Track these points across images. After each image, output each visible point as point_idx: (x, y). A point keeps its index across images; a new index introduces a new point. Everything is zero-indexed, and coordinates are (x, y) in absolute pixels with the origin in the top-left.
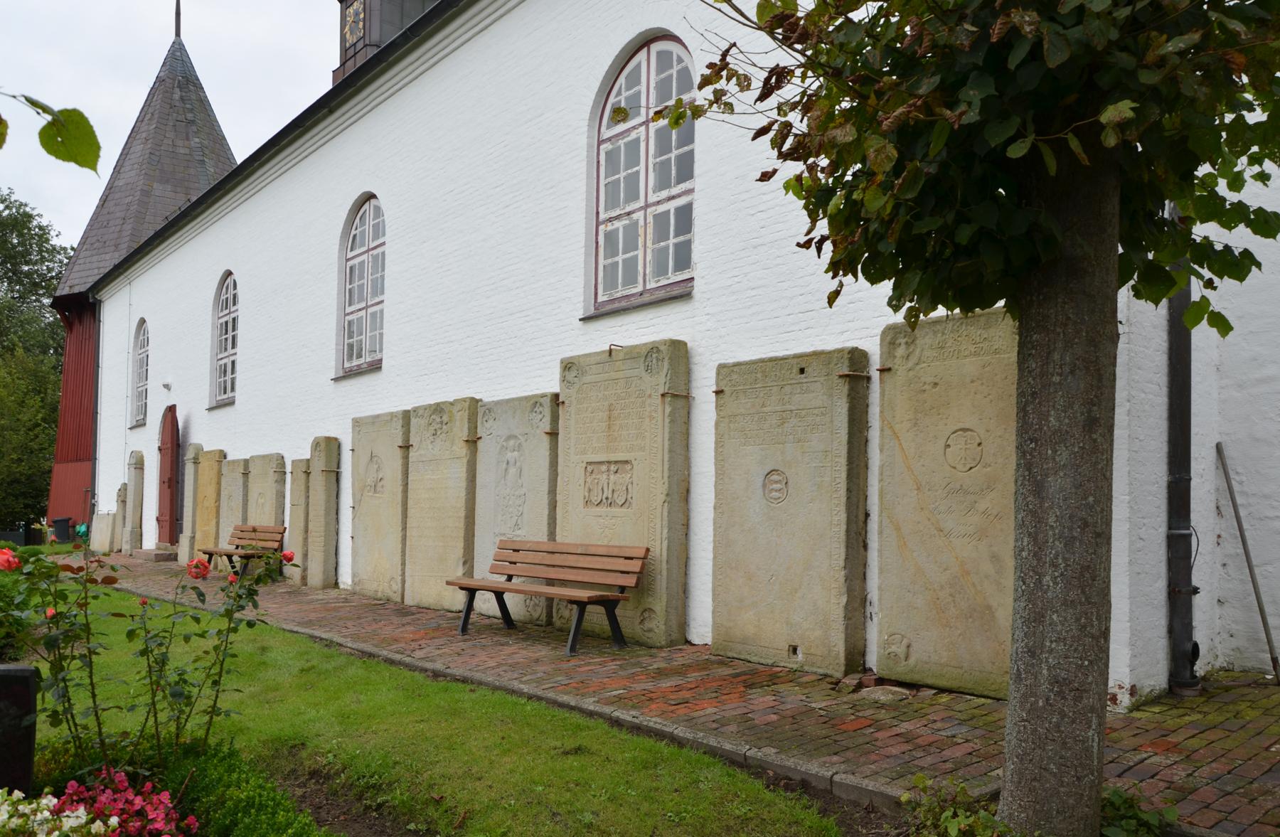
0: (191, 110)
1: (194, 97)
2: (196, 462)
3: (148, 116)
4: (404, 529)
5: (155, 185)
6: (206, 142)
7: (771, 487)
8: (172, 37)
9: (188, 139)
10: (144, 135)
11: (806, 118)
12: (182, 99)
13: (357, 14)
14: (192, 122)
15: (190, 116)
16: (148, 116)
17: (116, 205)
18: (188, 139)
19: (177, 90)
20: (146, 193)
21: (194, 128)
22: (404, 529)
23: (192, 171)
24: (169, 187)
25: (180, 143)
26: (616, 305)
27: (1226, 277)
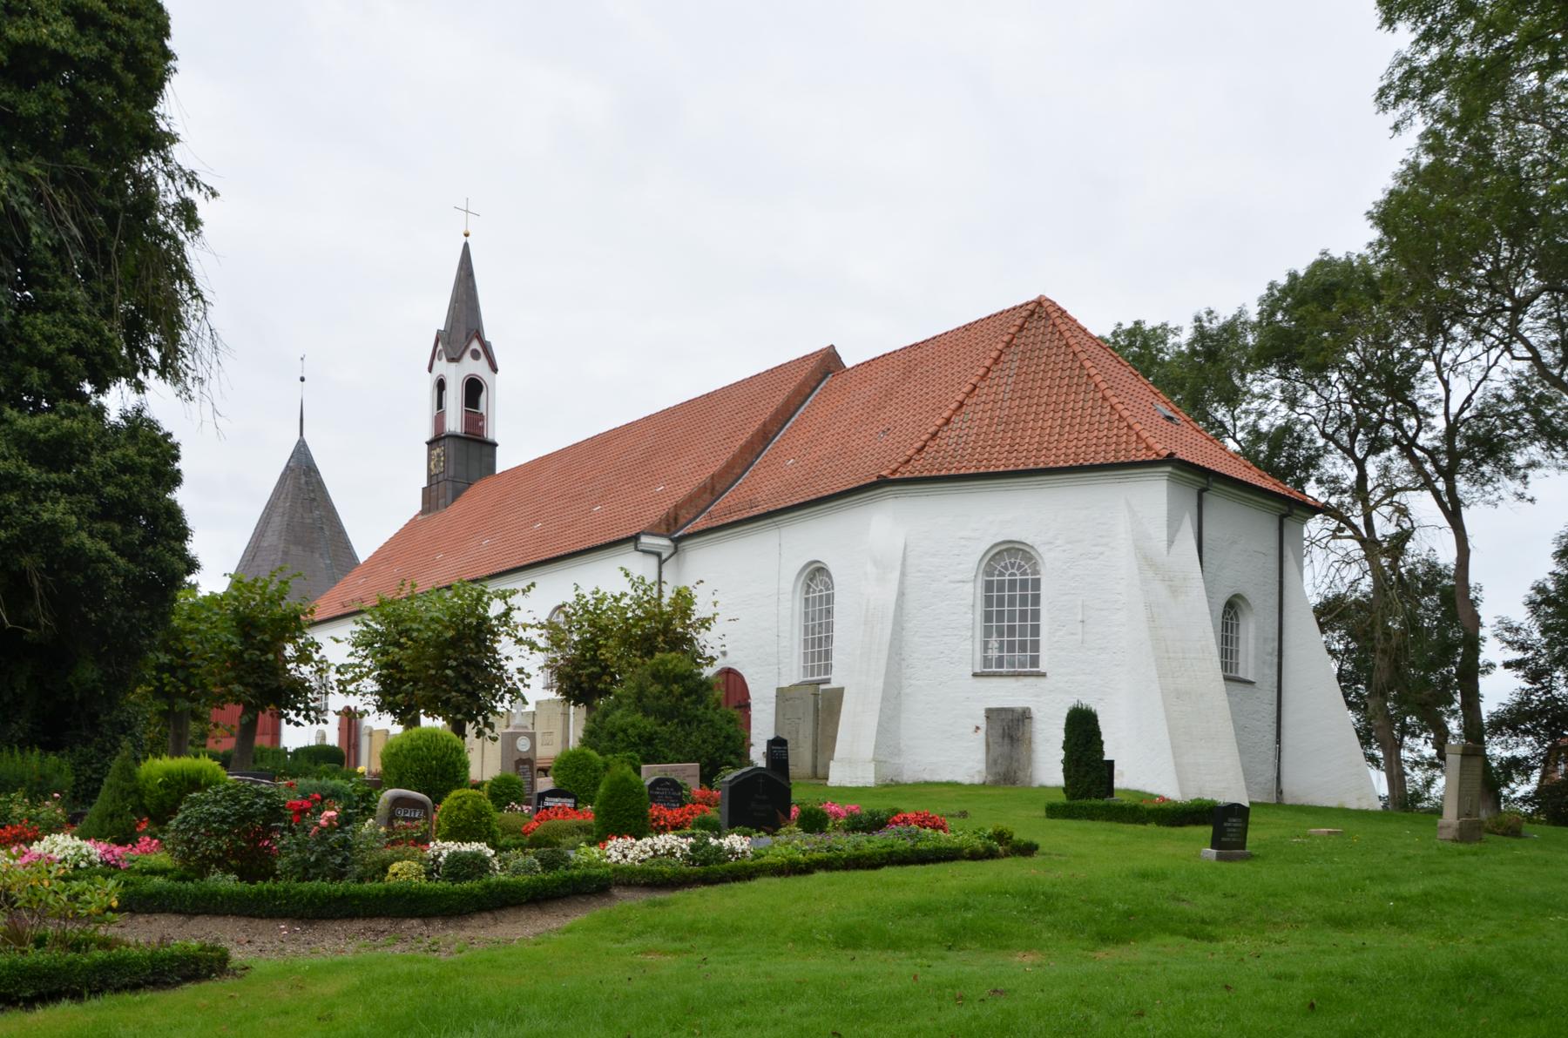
0: (313, 491)
1: (314, 480)
2: (370, 735)
3: (283, 496)
4: (483, 757)
5: (292, 547)
6: (323, 513)
7: (600, 758)
8: (297, 437)
9: (311, 512)
10: (281, 510)
11: (758, 755)
12: (307, 483)
13: (439, 456)
14: (314, 499)
15: (312, 495)
16: (283, 496)
17: (263, 560)
18: (311, 512)
19: (303, 477)
20: (285, 553)
21: (315, 504)
22: (483, 757)
23: (315, 535)
24: (300, 548)
25: (306, 515)
26: (353, 730)
27: (1106, 758)
